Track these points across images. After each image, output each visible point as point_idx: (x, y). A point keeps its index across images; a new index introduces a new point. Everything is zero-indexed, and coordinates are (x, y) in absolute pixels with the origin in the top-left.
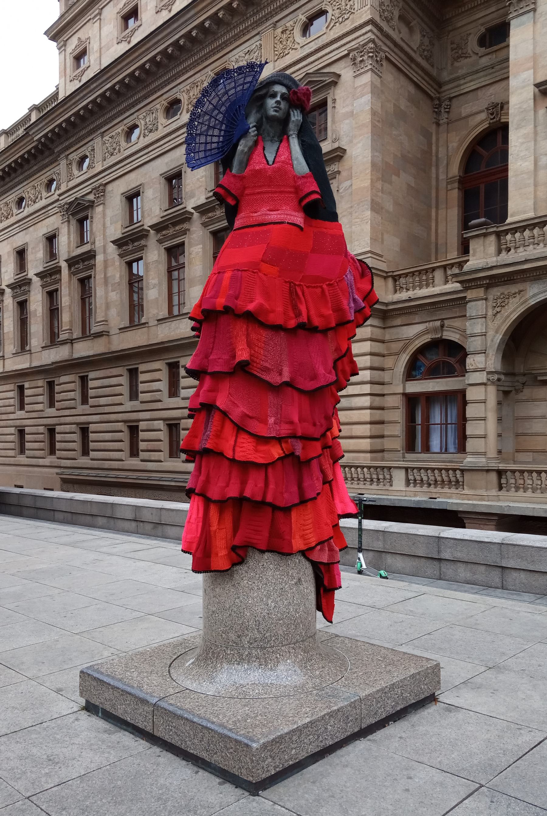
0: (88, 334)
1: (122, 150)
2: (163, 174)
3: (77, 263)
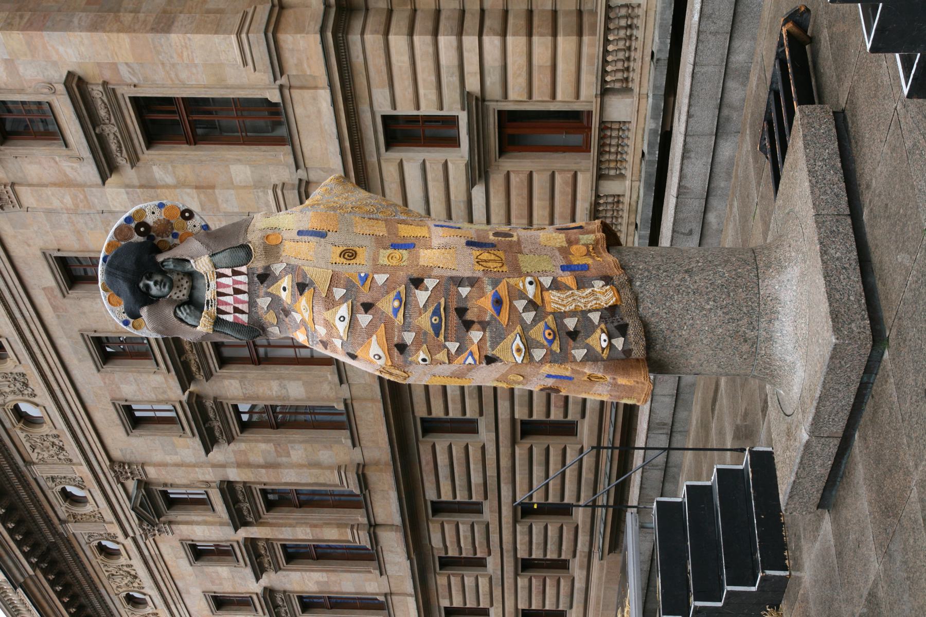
3: (239, 511)
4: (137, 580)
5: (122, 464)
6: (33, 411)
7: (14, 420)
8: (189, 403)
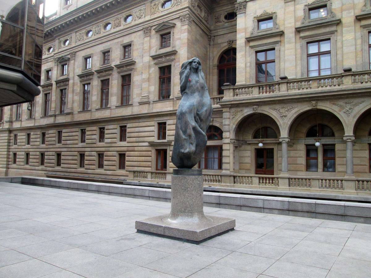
3: (60, 82)
5: (75, 55)
8: (92, 72)
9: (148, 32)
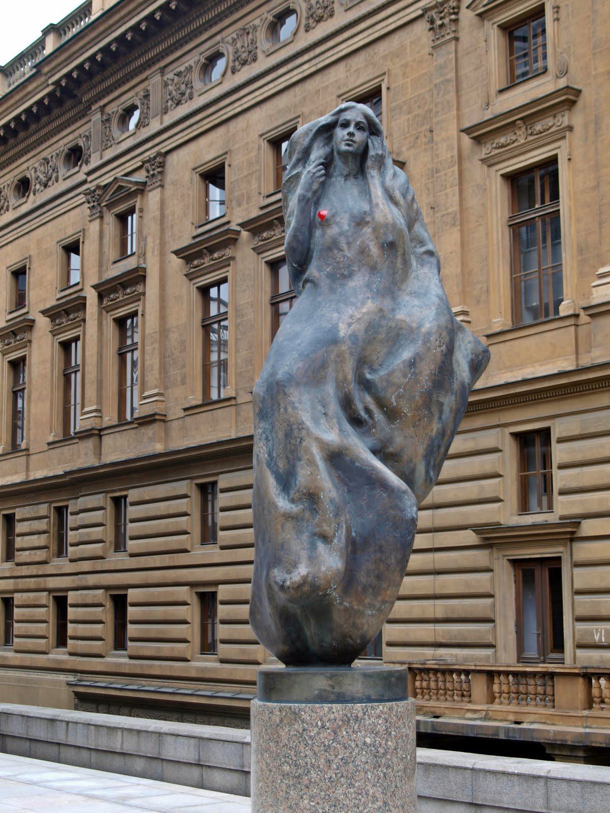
0: (128, 417)
1: (195, 95)
2: (10, 266)
3: (114, 290)
4: (42, 188)
5: (162, 165)
6: (286, 32)
7: (208, 53)
8: (228, 231)
9: (446, 21)
